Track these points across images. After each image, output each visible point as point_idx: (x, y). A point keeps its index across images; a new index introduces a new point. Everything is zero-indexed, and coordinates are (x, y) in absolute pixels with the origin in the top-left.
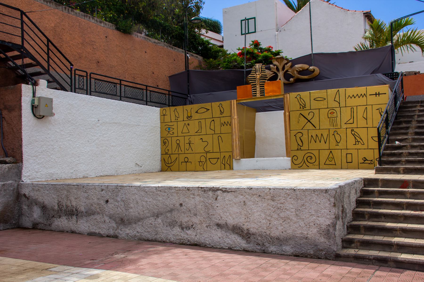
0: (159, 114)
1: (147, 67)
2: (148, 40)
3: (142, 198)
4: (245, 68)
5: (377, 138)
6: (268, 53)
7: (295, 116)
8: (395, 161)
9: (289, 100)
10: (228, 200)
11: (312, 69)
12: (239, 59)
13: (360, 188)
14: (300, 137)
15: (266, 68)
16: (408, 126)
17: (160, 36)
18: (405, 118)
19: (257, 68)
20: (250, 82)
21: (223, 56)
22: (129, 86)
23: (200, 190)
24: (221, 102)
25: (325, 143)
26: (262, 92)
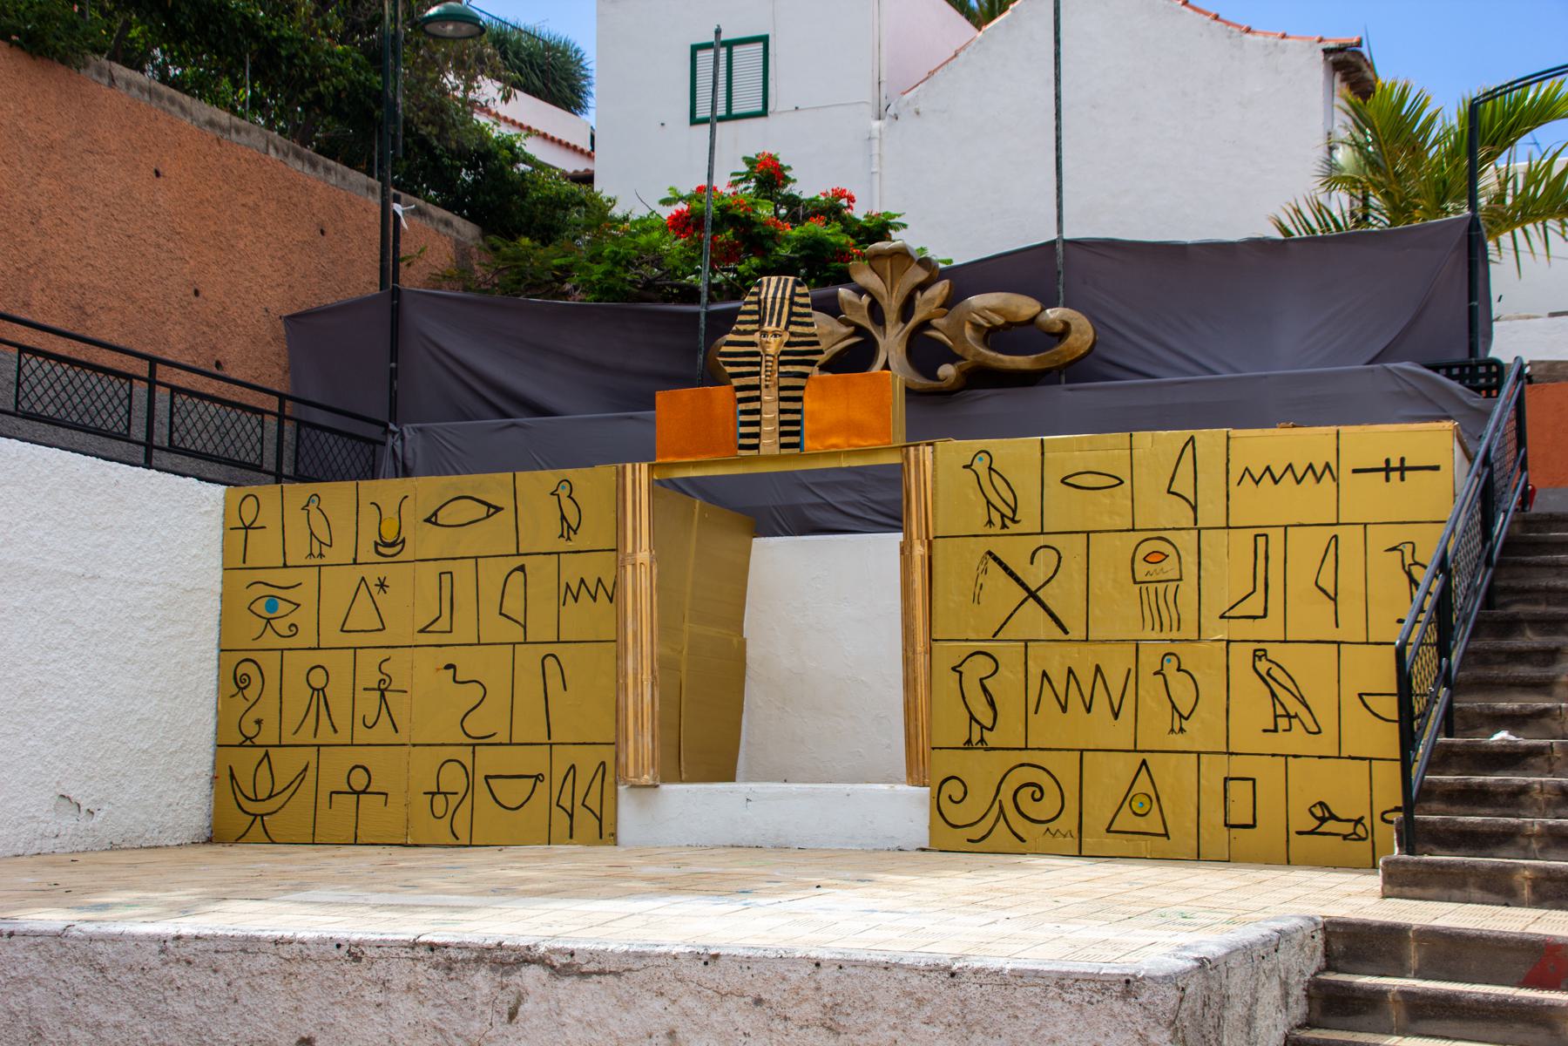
0: (216, 520)
1: (163, 255)
2: (176, 109)
3: (68, 1005)
4: (704, 299)
5: (1395, 699)
6: (827, 224)
7: (957, 563)
8: (1485, 829)
9: (934, 476)
10: (580, 1021)
11: (1053, 322)
12: (674, 246)
13: (1304, 975)
14: (981, 680)
15: (819, 305)
16: (1553, 646)
17: (246, 94)
18: (1537, 602)
19: (769, 300)
20: (729, 370)
21: (588, 228)
22: (48, 356)
23: (422, 959)
24: (569, 473)
25: (1116, 716)
26: (791, 430)
